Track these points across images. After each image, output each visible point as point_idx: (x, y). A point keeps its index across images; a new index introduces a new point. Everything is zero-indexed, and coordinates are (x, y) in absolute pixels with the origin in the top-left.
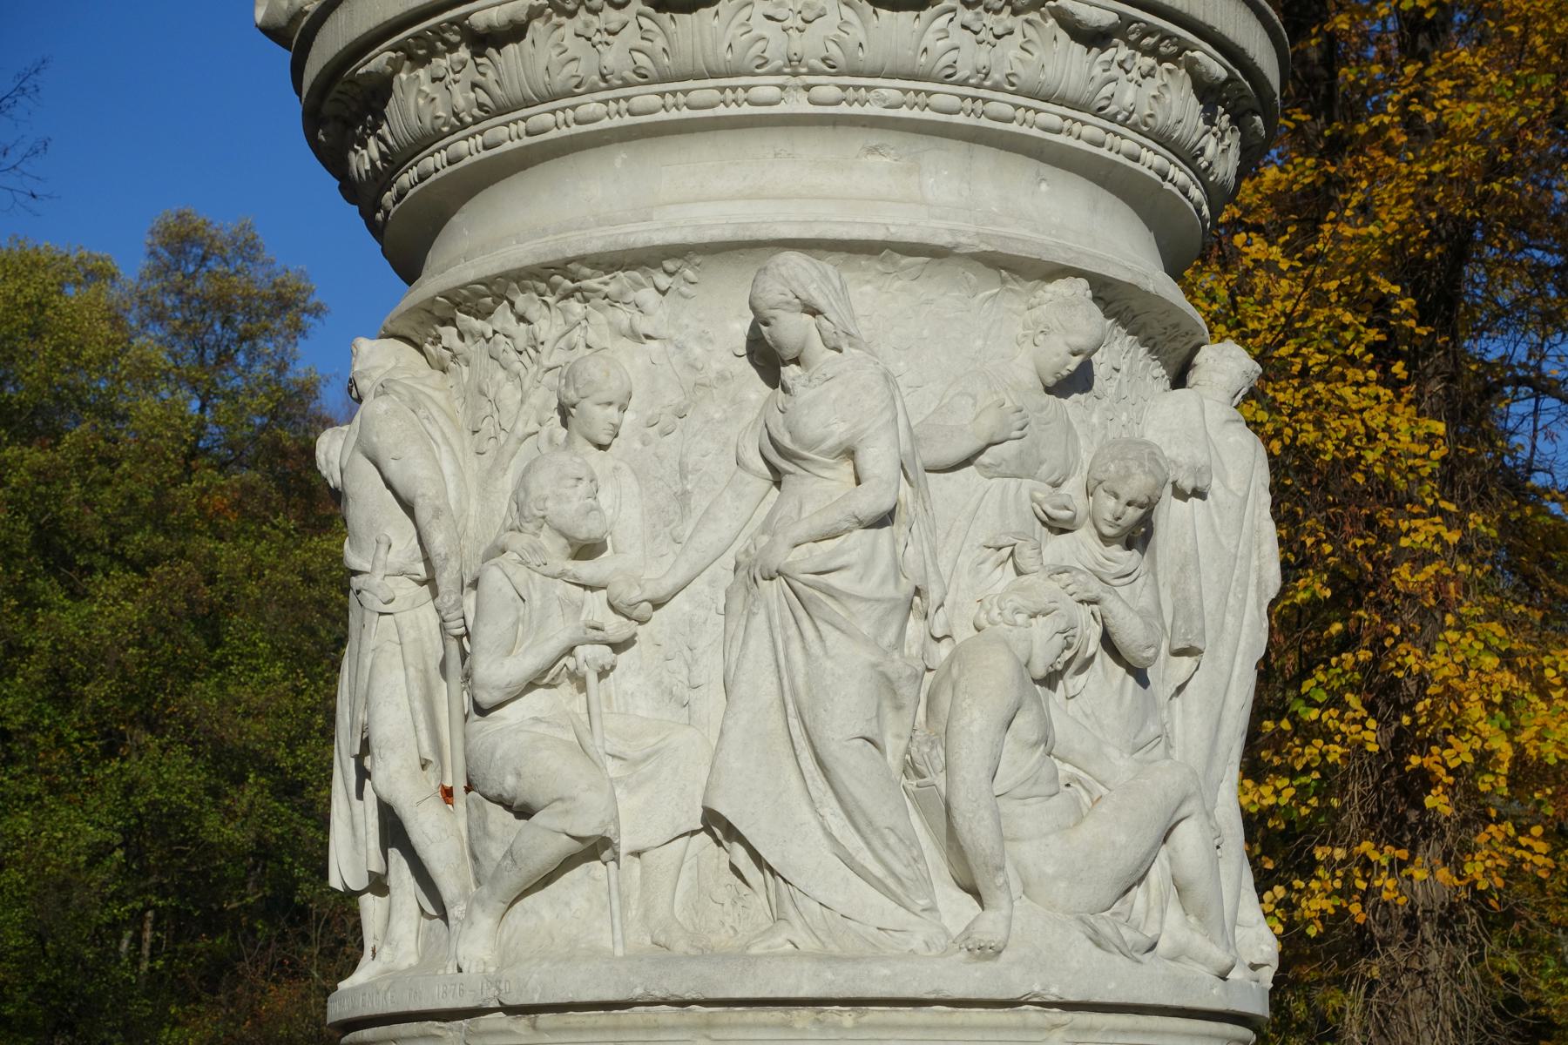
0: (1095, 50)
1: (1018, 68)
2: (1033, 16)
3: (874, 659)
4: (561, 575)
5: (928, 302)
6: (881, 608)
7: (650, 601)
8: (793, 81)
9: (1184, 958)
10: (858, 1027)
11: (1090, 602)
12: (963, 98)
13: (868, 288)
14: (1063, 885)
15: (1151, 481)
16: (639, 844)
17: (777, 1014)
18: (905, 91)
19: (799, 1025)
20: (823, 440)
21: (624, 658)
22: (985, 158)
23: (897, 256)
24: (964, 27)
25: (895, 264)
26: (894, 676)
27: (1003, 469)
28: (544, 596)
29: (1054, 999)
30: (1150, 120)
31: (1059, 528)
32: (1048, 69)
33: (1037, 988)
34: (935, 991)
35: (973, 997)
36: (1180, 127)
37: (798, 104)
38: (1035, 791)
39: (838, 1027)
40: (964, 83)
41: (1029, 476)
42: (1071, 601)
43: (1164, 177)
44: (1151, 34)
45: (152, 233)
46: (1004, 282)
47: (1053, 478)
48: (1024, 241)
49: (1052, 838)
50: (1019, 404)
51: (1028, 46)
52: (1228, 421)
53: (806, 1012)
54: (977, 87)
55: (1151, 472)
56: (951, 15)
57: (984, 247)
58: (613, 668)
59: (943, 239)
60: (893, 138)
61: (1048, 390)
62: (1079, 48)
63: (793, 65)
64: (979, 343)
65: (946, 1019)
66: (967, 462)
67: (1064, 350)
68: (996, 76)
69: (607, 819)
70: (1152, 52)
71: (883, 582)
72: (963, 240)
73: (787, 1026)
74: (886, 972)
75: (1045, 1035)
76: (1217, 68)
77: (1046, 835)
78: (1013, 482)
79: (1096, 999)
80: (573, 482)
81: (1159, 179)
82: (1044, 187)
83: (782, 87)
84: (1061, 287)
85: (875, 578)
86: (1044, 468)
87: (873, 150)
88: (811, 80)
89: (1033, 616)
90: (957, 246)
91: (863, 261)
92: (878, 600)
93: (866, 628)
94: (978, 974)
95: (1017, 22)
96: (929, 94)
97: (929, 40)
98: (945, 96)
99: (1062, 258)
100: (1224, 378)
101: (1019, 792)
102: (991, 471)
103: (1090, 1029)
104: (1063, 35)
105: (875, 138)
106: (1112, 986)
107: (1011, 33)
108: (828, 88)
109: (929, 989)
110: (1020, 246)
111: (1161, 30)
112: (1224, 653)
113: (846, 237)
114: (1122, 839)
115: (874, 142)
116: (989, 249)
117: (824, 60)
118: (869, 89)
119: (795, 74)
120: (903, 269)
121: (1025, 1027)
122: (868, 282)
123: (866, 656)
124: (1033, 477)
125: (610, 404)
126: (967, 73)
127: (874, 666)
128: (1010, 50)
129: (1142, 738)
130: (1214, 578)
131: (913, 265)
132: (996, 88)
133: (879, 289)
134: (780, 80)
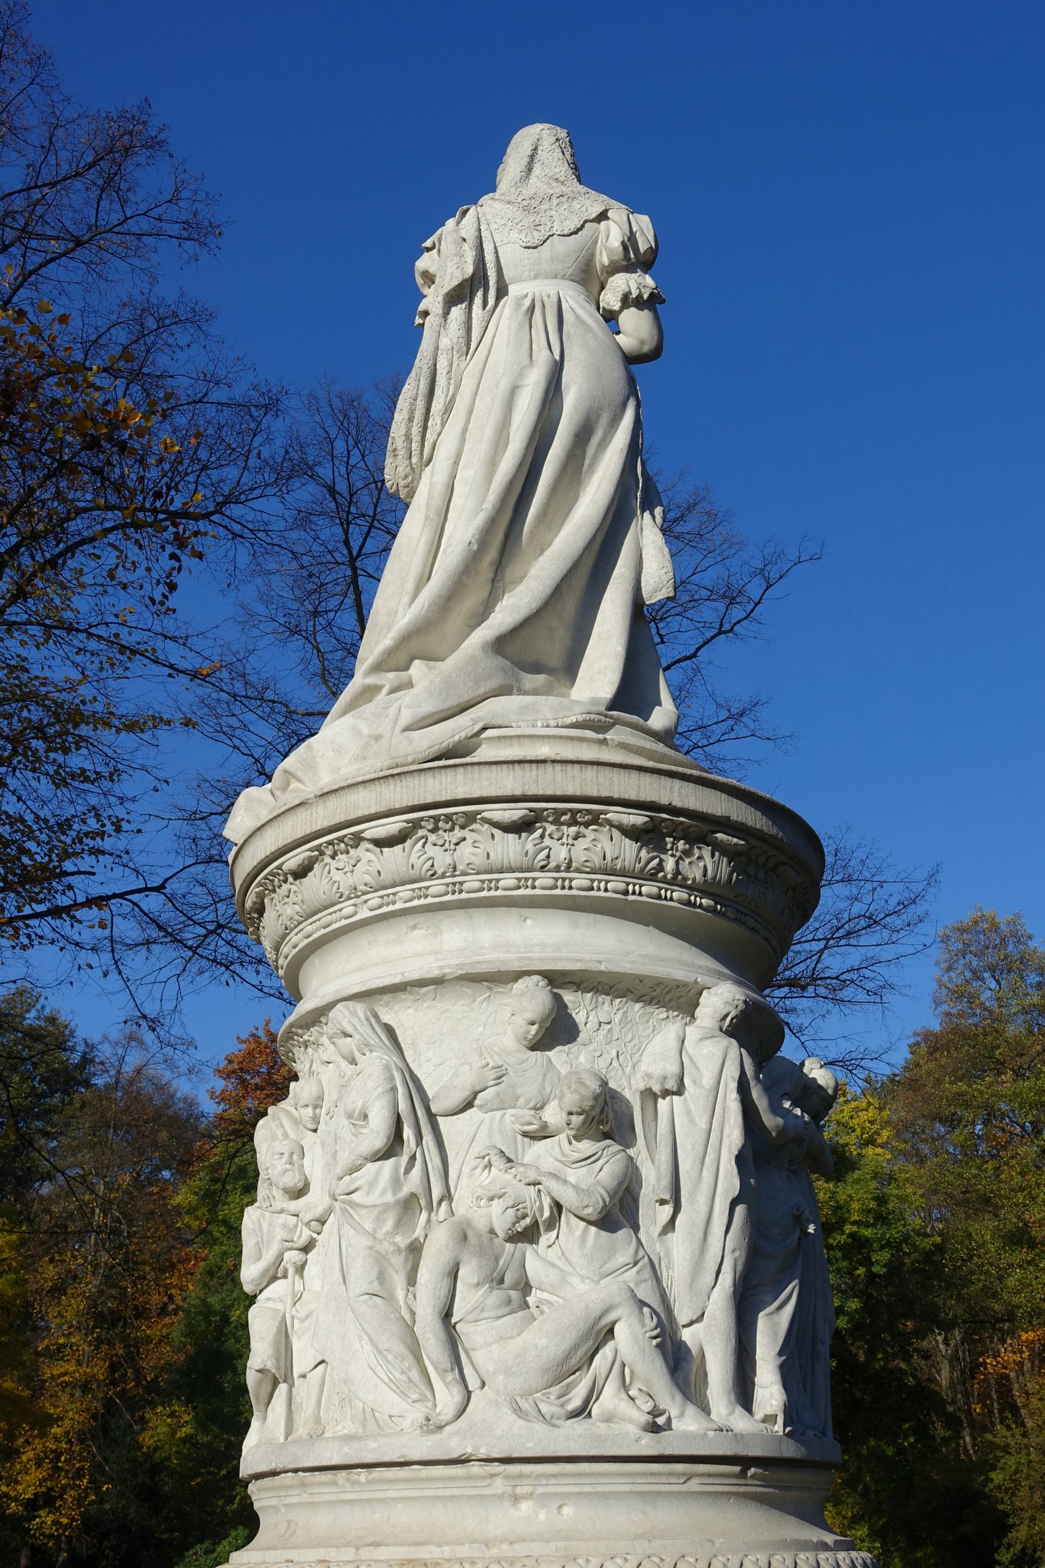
0: (524, 835)
1: (473, 859)
2: (474, 826)
3: (369, 1243)
4: (282, 1211)
5: (445, 1011)
6: (376, 1211)
7: (317, 1220)
8: (358, 901)
9: (616, 1420)
10: (369, 1482)
11: (535, 1184)
12: (447, 885)
13: (411, 1011)
14: (501, 1377)
15: (577, 1097)
16: (303, 1371)
17: (328, 1476)
18: (413, 890)
19: (340, 1482)
20: (354, 1112)
21: (310, 1256)
22: (480, 915)
23: (416, 989)
24: (435, 845)
25: (418, 993)
26: (384, 1252)
27: (489, 1106)
28: (270, 1225)
29: (484, 1457)
30: (587, 864)
31: (542, 1134)
32: (492, 855)
33: (469, 1450)
34: (402, 1456)
35: (374, 1461)
36: (619, 861)
37: (364, 913)
38: (483, 1315)
39: (358, 1482)
40: (443, 876)
41: (511, 1107)
42: (521, 1185)
43: (626, 893)
44: (565, 814)
45: (937, 963)
46: (490, 989)
47: (532, 1104)
48: (488, 962)
49: (495, 1345)
50: (500, 1063)
51: (476, 845)
52: (701, 1039)
53: (343, 1473)
54: (454, 876)
55: (575, 1091)
56: (424, 840)
57: (460, 972)
58: (305, 1262)
59: (435, 973)
60: (420, 918)
61: (533, 1048)
62: (511, 837)
63: (355, 892)
64: (481, 1029)
65: (416, 1474)
66: (469, 1105)
67: (523, 1023)
68: (460, 867)
69: (265, 1358)
70: (573, 822)
71: (383, 1193)
72: (447, 971)
73: (334, 1483)
74: (375, 1445)
75: (488, 1481)
76: (637, 819)
77: (490, 1344)
78: (499, 1113)
79: (516, 1455)
80: (278, 1156)
81: (623, 897)
82: (529, 922)
83: (355, 905)
84: (520, 985)
85: (377, 1192)
86: (521, 1100)
87: (414, 927)
88: (365, 897)
89: (491, 1199)
90: (444, 975)
91: (402, 996)
92: (373, 1206)
93: (368, 1226)
94: (429, 1443)
95: (465, 833)
96: (427, 888)
97: (413, 859)
98: (436, 886)
99: (517, 966)
100: (709, 1010)
101: (470, 1317)
102: (485, 1108)
103: (521, 1476)
104: (497, 832)
105: (411, 920)
106: (530, 1445)
107: (464, 839)
108: (374, 900)
109: (398, 1455)
110: (484, 966)
111: (570, 810)
112: (702, 1199)
113: (381, 985)
114: (543, 1342)
115: (412, 924)
116: (463, 972)
117: (366, 885)
118: (394, 894)
119: (358, 897)
120: (424, 995)
121: (469, 1477)
122: (409, 1007)
123: (366, 1242)
124: (514, 1107)
125: (307, 1106)
126: (442, 870)
127: (371, 1248)
128: (466, 849)
129: (610, 1266)
130: (689, 1147)
131: (429, 992)
132: (464, 874)
133: (416, 1010)
134: (352, 902)
